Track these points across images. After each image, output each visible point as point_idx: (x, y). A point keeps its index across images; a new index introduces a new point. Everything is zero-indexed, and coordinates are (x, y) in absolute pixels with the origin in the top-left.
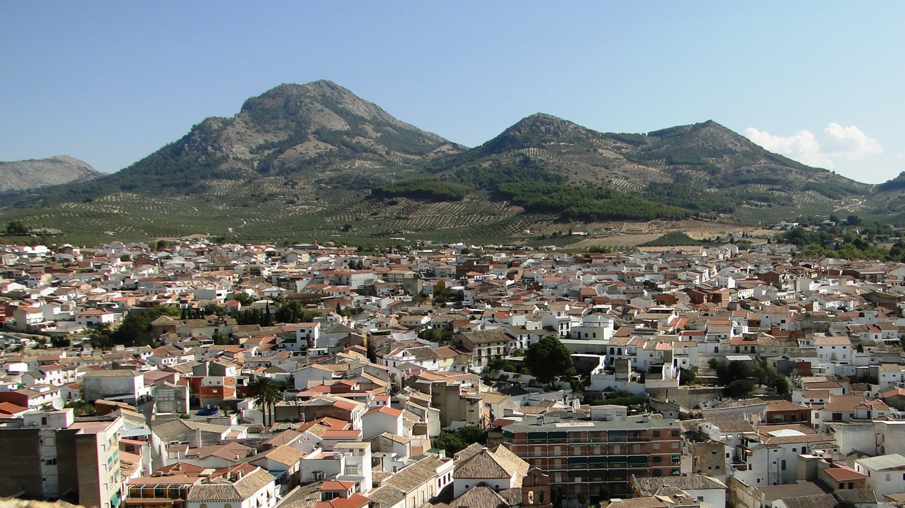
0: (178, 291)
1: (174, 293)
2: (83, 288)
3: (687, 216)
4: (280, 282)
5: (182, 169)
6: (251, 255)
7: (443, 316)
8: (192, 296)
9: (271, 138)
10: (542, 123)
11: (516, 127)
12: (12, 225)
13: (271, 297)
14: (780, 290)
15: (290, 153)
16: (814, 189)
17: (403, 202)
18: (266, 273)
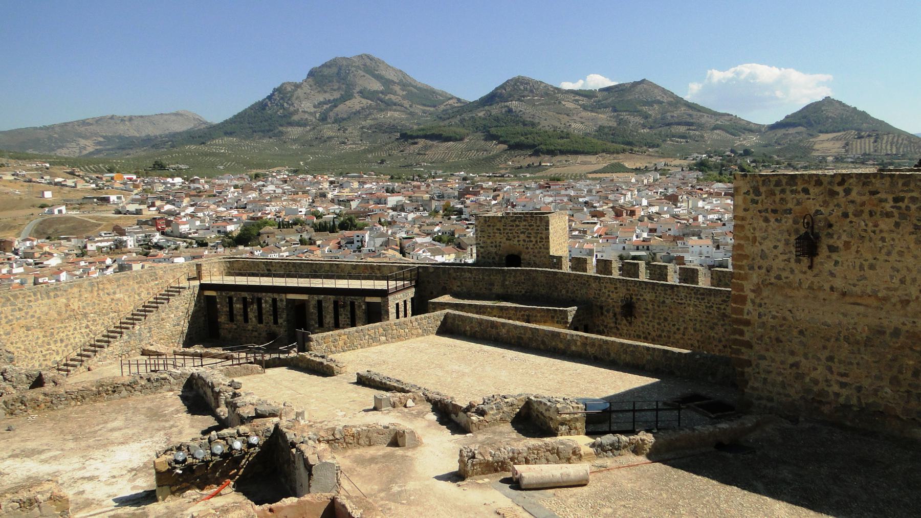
0: (273, 209)
1: (272, 209)
2: (212, 209)
3: (624, 151)
4: (340, 202)
5: (264, 120)
6: (319, 183)
7: (448, 226)
8: (284, 213)
9: (328, 96)
10: (522, 83)
11: (502, 87)
12: (156, 163)
13: (334, 213)
14: (677, 207)
15: (341, 108)
16: (720, 129)
17: (422, 142)
18: (330, 196)
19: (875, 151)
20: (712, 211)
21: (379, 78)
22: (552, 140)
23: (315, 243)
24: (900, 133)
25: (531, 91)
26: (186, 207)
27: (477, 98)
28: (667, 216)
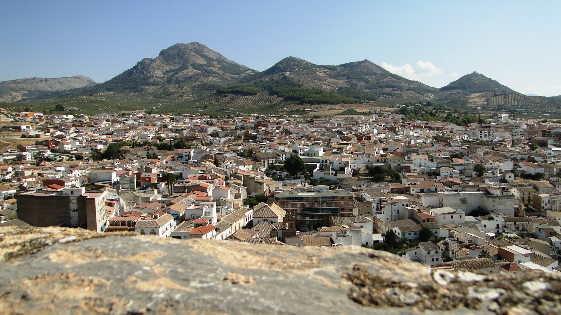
0: (131, 135)
1: (130, 135)
3: (355, 102)
4: (176, 131)
5: (133, 81)
6: (163, 119)
7: (248, 146)
8: (137, 137)
9: (172, 67)
10: (292, 61)
11: (280, 63)
13: (172, 138)
14: (397, 135)
15: (180, 74)
17: (230, 96)
18: (170, 127)
19: (505, 104)
21: (204, 57)
23: (157, 157)
25: (298, 66)
26: (72, 133)
27: (265, 70)
28: (391, 140)
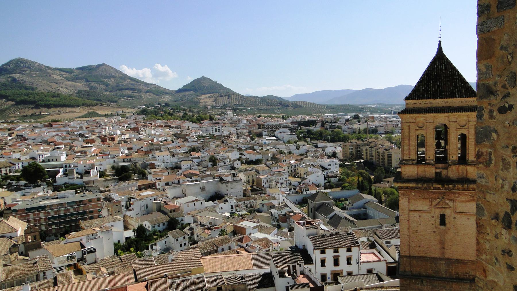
3: (97, 104)
10: (22, 62)
11: (8, 64)
20: (160, 136)
22: (48, 98)
24: (239, 95)
25: (29, 68)
